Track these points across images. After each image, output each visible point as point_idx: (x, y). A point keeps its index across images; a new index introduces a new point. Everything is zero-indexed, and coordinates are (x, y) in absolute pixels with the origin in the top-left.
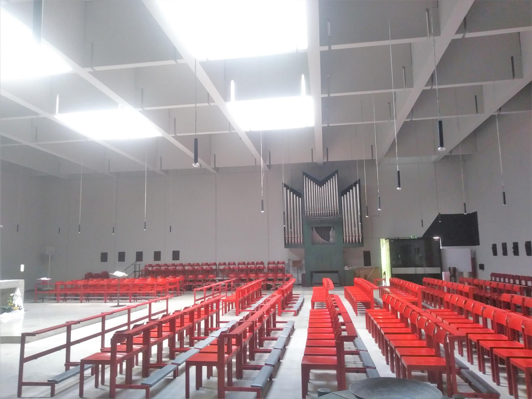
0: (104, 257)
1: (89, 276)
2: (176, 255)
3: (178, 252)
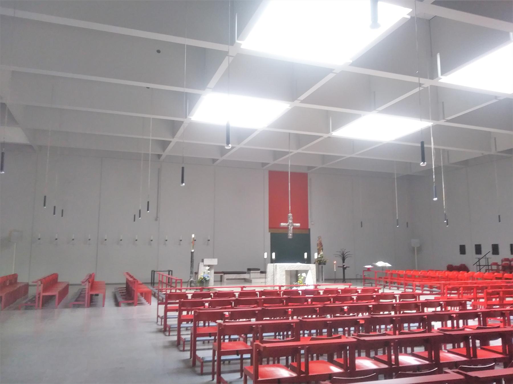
0: (463, 250)
1: (451, 268)
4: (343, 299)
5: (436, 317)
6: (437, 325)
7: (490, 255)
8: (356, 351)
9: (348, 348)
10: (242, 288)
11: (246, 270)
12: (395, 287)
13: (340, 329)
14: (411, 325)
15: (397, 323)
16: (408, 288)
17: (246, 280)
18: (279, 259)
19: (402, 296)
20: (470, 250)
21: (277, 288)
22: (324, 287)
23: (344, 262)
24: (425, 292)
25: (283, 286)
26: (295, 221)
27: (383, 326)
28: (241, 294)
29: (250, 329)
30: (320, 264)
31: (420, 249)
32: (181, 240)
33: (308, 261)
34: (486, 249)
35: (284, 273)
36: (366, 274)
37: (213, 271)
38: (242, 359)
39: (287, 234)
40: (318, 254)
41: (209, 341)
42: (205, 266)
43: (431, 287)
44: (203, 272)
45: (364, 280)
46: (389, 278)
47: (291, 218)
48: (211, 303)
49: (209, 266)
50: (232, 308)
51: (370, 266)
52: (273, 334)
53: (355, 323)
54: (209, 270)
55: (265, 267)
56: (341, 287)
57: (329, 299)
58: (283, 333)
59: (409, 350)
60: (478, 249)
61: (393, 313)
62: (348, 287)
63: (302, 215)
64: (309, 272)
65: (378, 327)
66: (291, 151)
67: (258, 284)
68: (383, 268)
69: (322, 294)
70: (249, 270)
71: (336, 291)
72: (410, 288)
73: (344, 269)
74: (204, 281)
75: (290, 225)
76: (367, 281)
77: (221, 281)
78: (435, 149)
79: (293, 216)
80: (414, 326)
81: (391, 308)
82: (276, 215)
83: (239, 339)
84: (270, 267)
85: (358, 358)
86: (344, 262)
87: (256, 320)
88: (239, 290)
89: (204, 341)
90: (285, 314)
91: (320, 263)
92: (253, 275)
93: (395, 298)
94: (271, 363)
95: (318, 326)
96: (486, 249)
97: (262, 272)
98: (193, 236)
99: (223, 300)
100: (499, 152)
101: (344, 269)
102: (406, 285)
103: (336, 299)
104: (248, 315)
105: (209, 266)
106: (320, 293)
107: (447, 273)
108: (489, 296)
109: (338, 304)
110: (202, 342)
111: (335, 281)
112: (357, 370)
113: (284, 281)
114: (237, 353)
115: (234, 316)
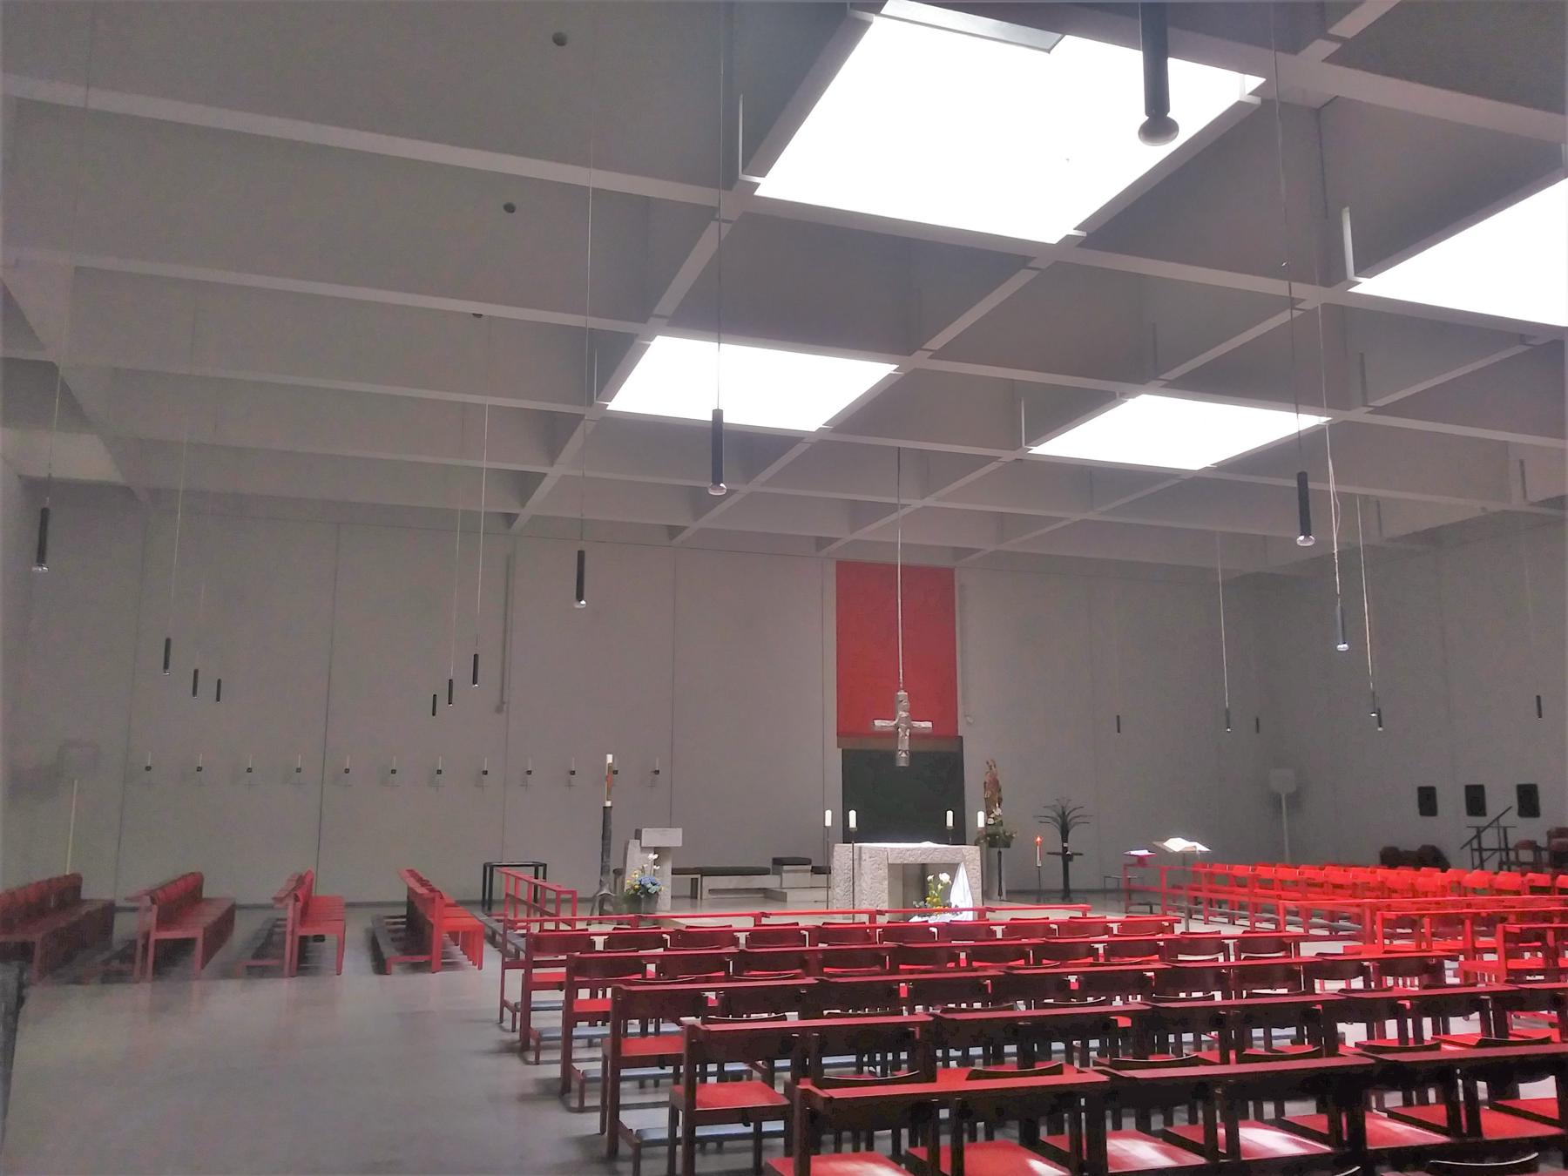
0: (1427, 801)
1: (1392, 858)
2: (1528, 801)
3: (1480, 788)
4: (1063, 953)
5: (1349, 1008)
6: (1353, 1033)
7: (1512, 818)
8: (1108, 1113)
9: (1083, 1102)
10: (757, 918)
11: (769, 865)
12: (1221, 914)
13: (1058, 1046)
14: (1275, 1032)
15: (1231, 1027)
16: (1260, 921)
17: (767, 894)
18: (867, 832)
19: (1244, 943)
20: (1451, 801)
21: (865, 918)
22: (1006, 916)
23: (1065, 840)
24: (1313, 932)
25: (881, 913)
26: (915, 715)
27: (1188, 1037)
28: (755, 936)
29: (784, 1043)
30: (992, 844)
31: (1295, 800)
32: (657, 772)
33: (958, 836)
34: (1501, 799)
35: (884, 872)
36: (1135, 875)
37: (668, 867)
38: (759, 1135)
39: (891, 756)
40: (988, 814)
41: (657, 1079)
42: (645, 849)
43: (1333, 916)
44: (639, 867)
45: (1127, 893)
46: (1199, 886)
47: (905, 703)
48: (664, 965)
49: (656, 850)
50: (728, 979)
51: (1145, 852)
52: (852, 1059)
53: (1103, 1026)
54: (656, 862)
55: (828, 854)
56: (1058, 915)
57: (1021, 953)
58: (884, 1057)
59: (1269, 1109)
60: (1475, 800)
61: (1218, 995)
62: (1079, 914)
63: (939, 695)
64: (962, 873)
65: (1172, 1038)
66: (903, 501)
67: (804, 907)
68: (1185, 856)
69: (999, 936)
70: (779, 862)
71: (1044, 927)
72: (1268, 920)
73: (1067, 858)
74: (643, 896)
75: (902, 726)
76: (1136, 898)
77: (694, 896)
78: (1339, 493)
79: (910, 697)
80: (1283, 1036)
81: (1210, 980)
82: (859, 695)
83: (749, 1073)
84: (842, 854)
85: (1115, 1137)
86: (1065, 840)
87: (801, 1017)
88: (749, 923)
89: (642, 1081)
90: (886, 997)
91: (994, 841)
92: (791, 878)
93: (1224, 949)
94: (847, 1148)
95: (991, 1036)
96: (1501, 799)
97: (816, 871)
98: (610, 758)
99: (701, 952)
100: (1532, 504)
101: (1067, 858)
102: (1256, 908)
103: (1043, 952)
104: (776, 1001)
105: (656, 850)
106: (994, 933)
107: (1383, 873)
108: (1514, 944)
109: (1049, 967)
110: (636, 1084)
111: (1039, 896)
112: (1111, 1170)
113: (885, 896)
114: (743, 1116)
115: (734, 1004)
